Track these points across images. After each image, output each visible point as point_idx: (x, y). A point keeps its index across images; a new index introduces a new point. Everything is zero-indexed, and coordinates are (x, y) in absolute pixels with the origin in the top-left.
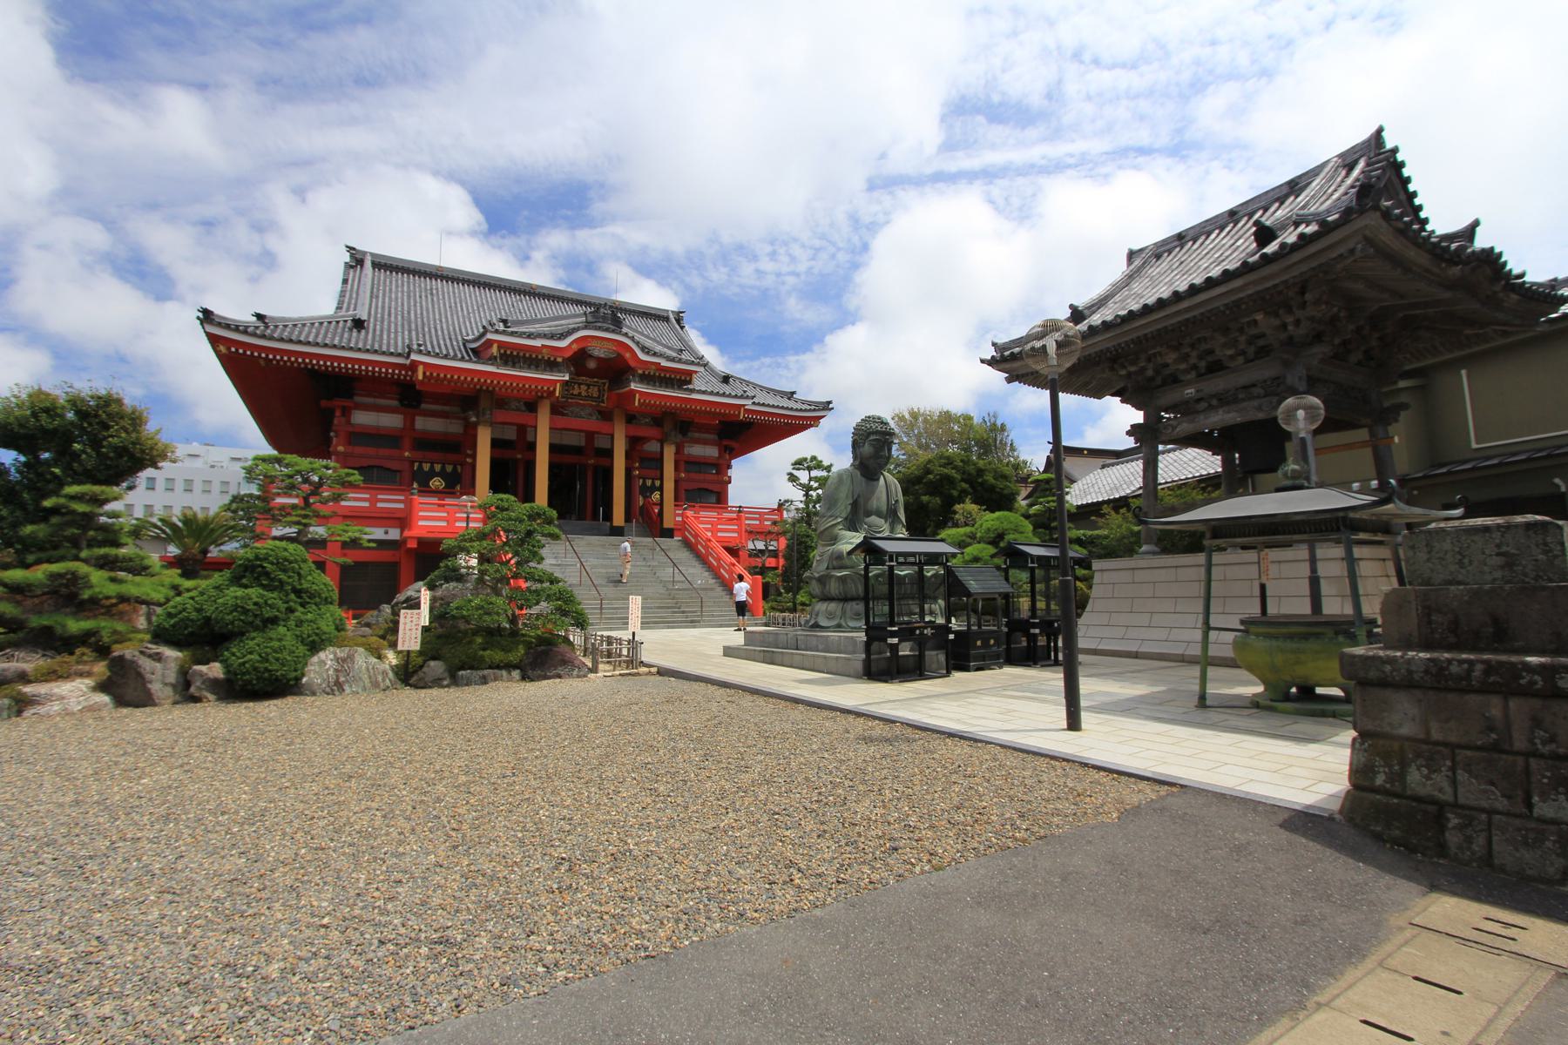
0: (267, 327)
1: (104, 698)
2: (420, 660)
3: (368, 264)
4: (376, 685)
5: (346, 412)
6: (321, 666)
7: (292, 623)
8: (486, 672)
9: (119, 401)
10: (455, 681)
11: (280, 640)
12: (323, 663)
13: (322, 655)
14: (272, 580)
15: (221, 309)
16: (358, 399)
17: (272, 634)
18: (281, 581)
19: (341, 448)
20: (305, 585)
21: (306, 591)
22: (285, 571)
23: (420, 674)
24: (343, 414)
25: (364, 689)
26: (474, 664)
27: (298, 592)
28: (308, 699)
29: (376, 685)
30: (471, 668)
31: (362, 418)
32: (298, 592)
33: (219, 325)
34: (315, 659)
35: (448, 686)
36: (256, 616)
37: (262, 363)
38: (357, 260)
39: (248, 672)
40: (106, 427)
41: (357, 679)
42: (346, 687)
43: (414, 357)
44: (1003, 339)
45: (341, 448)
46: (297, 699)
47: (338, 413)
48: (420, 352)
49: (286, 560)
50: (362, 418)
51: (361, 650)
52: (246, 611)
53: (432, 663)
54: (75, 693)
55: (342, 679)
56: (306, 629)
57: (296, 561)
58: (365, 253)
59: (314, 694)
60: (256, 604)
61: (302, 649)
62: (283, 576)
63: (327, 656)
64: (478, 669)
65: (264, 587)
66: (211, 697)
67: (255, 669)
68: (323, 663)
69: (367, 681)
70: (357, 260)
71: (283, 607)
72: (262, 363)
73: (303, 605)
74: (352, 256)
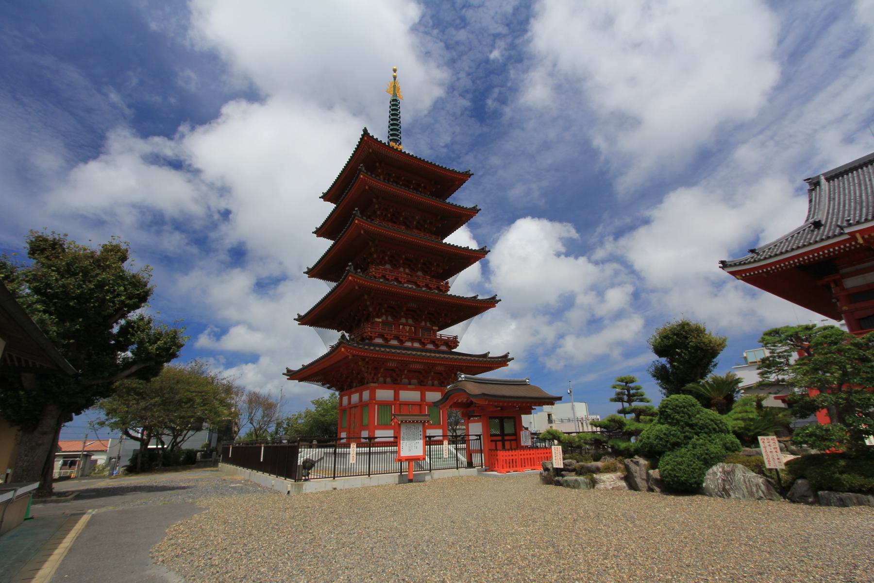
0: (758, 254)
1: (624, 484)
2: (789, 478)
3: (823, 181)
4: (751, 494)
5: (838, 283)
6: (715, 475)
7: (690, 446)
8: (845, 495)
9: (688, 324)
10: (818, 501)
11: (682, 457)
12: (715, 473)
13: (715, 468)
14: (673, 419)
15: (296, 366)
16: (842, 271)
17: (678, 453)
18: (677, 419)
19: (845, 308)
20: (694, 421)
21: (696, 425)
22: (678, 413)
23: (792, 489)
24: (836, 285)
25: (744, 497)
26: (834, 486)
27: (691, 426)
28: (706, 498)
29: (751, 494)
30: (830, 489)
31: (851, 283)
32: (691, 426)
33: (731, 266)
34: (710, 471)
35: (812, 504)
36: (667, 442)
37: (765, 275)
38: (814, 183)
39: (666, 477)
40: (686, 338)
41: (737, 489)
42: (731, 493)
43: (847, 231)
44: (327, 184)
45: (845, 308)
46: (700, 497)
47: (832, 286)
48: (850, 225)
49: (677, 406)
50: (851, 283)
51: (740, 466)
52: (661, 439)
53: (800, 481)
54: (609, 480)
55: (727, 487)
56: (698, 451)
57: (684, 407)
58: (818, 177)
59: (711, 495)
60: (665, 434)
61: (699, 463)
62: (678, 417)
63: (717, 469)
64: (836, 491)
65: (669, 423)
66: (657, 489)
67: (670, 474)
68: (715, 473)
69: (745, 490)
70: (814, 183)
71: (682, 436)
72: (765, 275)
73: (697, 434)
74: (810, 184)
